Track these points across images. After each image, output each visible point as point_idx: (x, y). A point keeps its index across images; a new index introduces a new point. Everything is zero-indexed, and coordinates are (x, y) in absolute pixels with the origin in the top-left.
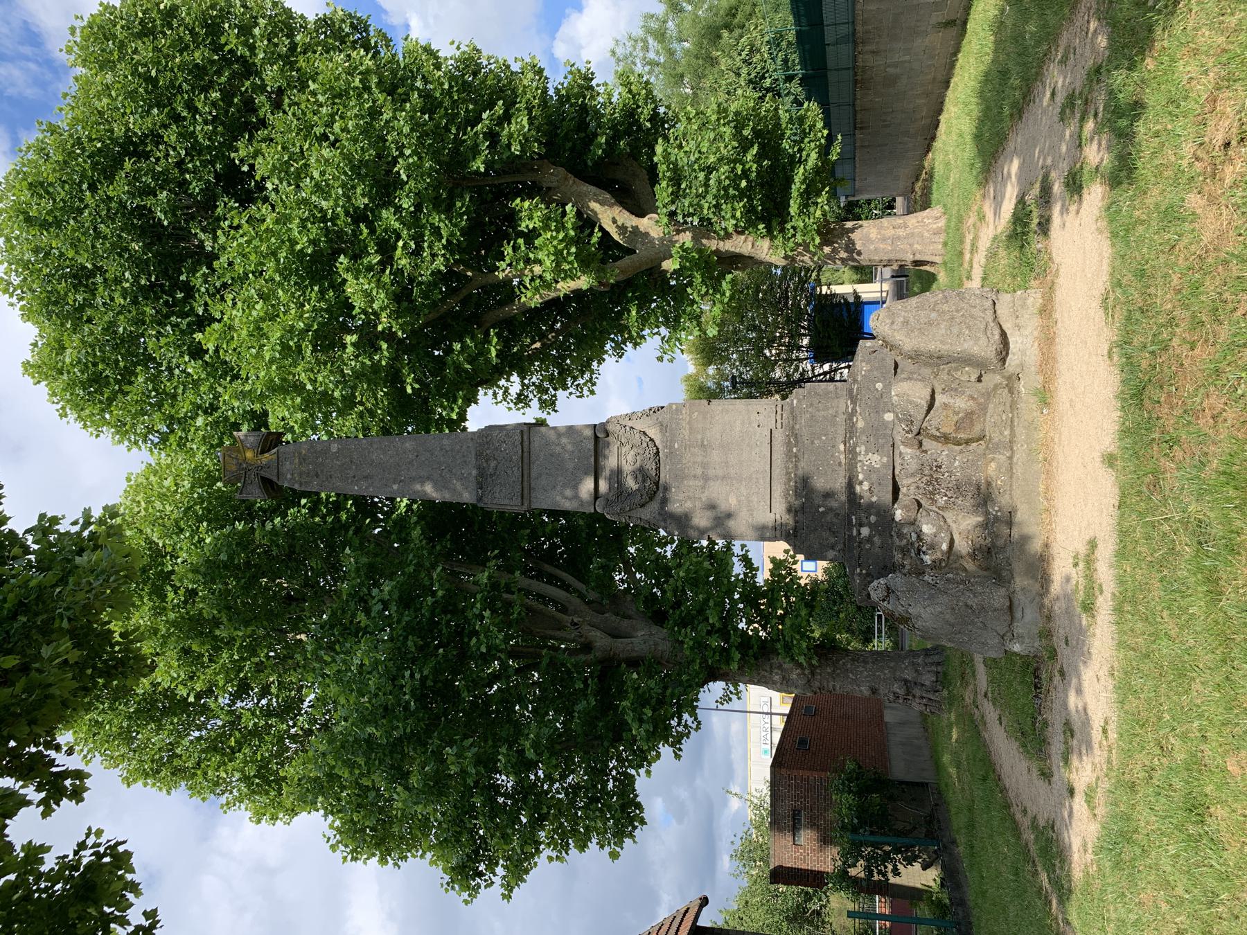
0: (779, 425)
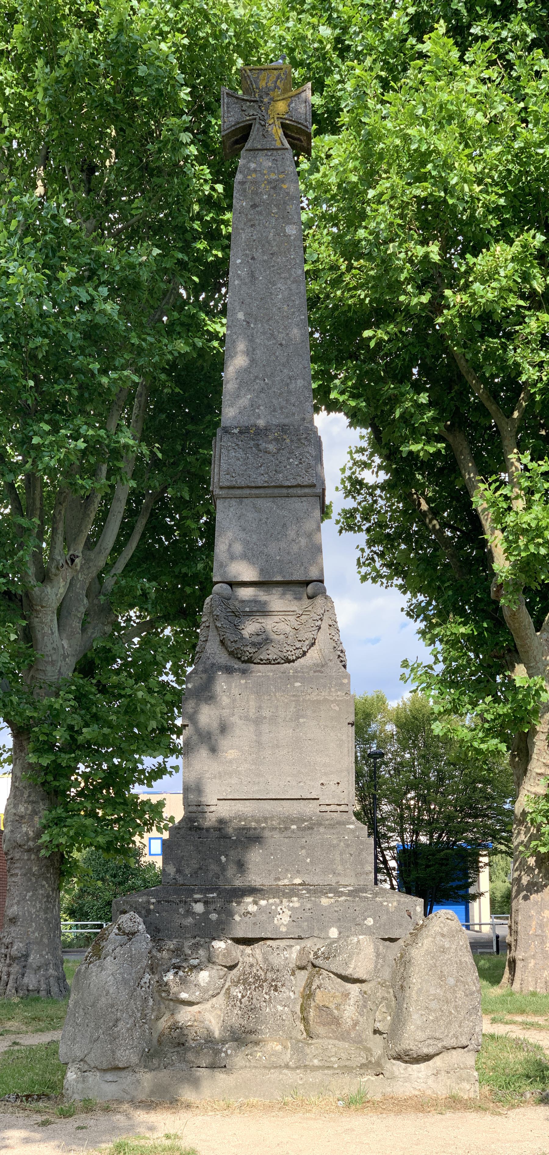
0: (324, 808)
